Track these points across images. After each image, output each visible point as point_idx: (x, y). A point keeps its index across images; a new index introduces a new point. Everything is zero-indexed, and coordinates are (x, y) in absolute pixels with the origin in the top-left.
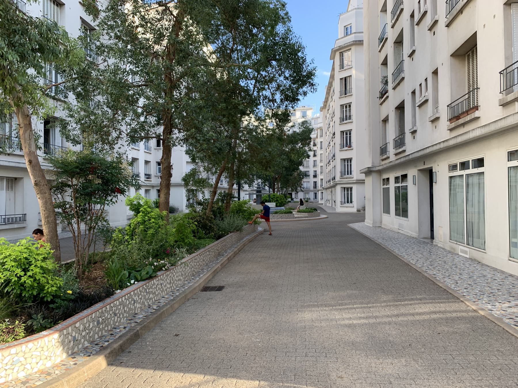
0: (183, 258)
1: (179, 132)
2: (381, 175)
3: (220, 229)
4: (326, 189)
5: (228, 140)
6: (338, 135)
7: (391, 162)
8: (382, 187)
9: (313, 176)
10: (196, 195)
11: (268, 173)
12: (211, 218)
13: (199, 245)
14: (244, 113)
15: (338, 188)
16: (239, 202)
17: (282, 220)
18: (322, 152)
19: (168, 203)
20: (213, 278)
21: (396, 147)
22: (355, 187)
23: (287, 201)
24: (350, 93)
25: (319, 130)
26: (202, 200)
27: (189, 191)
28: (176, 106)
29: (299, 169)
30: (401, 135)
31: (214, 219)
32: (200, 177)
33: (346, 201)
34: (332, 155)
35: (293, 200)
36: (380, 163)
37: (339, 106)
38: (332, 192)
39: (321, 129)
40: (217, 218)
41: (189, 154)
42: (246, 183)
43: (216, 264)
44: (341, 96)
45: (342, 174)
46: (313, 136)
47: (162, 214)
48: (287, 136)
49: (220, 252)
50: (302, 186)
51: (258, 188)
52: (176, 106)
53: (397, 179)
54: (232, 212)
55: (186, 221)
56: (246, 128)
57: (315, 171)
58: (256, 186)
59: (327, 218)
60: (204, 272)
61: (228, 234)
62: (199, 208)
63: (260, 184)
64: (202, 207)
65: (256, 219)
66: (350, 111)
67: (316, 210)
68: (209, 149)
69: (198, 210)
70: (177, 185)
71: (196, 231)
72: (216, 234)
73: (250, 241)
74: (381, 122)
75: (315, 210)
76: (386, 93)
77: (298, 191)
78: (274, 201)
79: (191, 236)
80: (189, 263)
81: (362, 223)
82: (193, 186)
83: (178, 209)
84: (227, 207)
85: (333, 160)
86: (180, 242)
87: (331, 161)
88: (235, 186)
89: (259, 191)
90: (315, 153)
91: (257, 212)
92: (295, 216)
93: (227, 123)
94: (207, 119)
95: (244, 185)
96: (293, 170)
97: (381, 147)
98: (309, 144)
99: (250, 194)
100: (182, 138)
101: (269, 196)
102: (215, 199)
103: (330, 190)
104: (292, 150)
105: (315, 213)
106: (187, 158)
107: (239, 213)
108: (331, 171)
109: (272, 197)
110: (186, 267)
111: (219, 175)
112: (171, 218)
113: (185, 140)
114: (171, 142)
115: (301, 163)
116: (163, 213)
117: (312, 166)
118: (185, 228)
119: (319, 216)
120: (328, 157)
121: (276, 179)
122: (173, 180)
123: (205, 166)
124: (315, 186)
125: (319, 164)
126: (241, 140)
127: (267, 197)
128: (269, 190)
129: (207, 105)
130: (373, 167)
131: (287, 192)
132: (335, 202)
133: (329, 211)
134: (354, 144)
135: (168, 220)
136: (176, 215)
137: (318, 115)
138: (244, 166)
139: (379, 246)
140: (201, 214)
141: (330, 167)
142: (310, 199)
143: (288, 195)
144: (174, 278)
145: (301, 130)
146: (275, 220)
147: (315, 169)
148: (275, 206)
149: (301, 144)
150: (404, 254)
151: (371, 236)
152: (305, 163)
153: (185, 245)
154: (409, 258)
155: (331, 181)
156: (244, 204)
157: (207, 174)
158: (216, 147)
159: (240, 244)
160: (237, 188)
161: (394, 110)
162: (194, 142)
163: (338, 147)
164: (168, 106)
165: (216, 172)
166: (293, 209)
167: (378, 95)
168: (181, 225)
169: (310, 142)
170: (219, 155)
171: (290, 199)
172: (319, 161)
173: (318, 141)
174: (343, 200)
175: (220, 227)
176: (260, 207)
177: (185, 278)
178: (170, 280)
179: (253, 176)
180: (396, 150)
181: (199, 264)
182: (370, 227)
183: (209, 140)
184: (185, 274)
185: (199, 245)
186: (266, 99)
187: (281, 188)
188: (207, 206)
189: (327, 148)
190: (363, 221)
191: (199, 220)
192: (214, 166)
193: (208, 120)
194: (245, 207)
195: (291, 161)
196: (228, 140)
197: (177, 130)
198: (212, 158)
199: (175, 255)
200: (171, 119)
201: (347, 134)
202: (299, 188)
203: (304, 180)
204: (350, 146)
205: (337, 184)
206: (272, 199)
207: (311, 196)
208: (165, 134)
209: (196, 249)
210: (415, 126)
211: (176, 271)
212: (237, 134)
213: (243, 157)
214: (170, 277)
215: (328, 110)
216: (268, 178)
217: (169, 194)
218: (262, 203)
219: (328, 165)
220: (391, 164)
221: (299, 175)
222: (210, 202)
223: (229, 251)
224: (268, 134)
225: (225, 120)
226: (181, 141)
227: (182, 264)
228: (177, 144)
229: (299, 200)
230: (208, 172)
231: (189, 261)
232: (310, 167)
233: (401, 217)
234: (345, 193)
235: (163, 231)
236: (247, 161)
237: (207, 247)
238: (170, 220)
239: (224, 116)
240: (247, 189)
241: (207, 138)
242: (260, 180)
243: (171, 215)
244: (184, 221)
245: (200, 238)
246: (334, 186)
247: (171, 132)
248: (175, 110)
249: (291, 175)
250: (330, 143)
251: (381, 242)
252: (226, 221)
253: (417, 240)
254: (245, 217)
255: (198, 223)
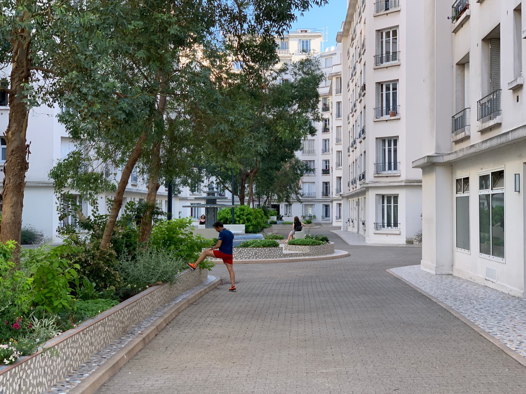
0: (48, 338)
1: (46, 77)
2: (452, 173)
3: (129, 279)
4: (348, 197)
5: (148, 97)
6: (371, 90)
7: (472, 146)
8: (455, 196)
9: (321, 172)
10: (80, 206)
11: (229, 164)
12: (111, 255)
13: (83, 312)
14: (180, 42)
15: (371, 197)
16: (169, 223)
17: (258, 260)
18: (340, 123)
19: (20, 223)
20: (110, 380)
21: (482, 117)
22: (403, 195)
23: (269, 221)
24: (395, 6)
25: (334, 79)
26: (92, 218)
27: (66, 198)
28: (38, 23)
29: (293, 156)
30: (493, 93)
31: (117, 258)
32: (90, 170)
33: (386, 221)
34: (359, 130)
35: (281, 219)
36: (451, 149)
37: (374, 33)
38: (358, 204)
39: (338, 76)
40: (122, 256)
41: (66, 122)
42: (185, 183)
43: (118, 352)
44: (377, 12)
45: (379, 169)
46: (322, 90)
47: (5, 247)
48: (270, 89)
49: (127, 326)
50: (300, 191)
51: (209, 194)
52: (38, 23)
53: (483, 179)
54: (154, 243)
55: (57, 261)
56: (184, 71)
57: (327, 162)
58: (206, 189)
59: (348, 255)
60: (91, 367)
61: (145, 289)
62: (84, 235)
63: (214, 186)
64: (91, 232)
65: (205, 258)
66: (395, 43)
67: (325, 239)
68: (105, 114)
69: (83, 238)
70: (40, 186)
71: (77, 283)
72: (120, 288)
73: (192, 303)
74: (455, 66)
75: (325, 239)
76: (465, 9)
77: (291, 200)
78: (241, 221)
79: (66, 293)
80: (61, 349)
81: (415, 266)
82: (73, 188)
83: (42, 235)
84: (143, 234)
85: (361, 139)
86: (43, 305)
87: (358, 141)
88: (163, 190)
89: (211, 201)
90: (326, 125)
91: (205, 244)
92: (285, 252)
93: (147, 61)
94: (104, 52)
95: (181, 188)
96: (283, 159)
97: (453, 117)
98: (314, 107)
99: (193, 208)
100: (50, 89)
101: (232, 210)
102: (120, 215)
103: (356, 199)
104: (280, 117)
105: (324, 246)
106: (62, 130)
107: (169, 245)
108: (358, 161)
109: (238, 213)
110: (55, 358)
111: (127, 168)
112: (23, 255)
113: (57, 94)
114: (27, 97)
115: (296, 145)
116: (8, 245)
117: (321, 151)
118: (54, 275)
119: (333, 252)
120: (351, 134)
121: (247, 175)
122: (30, 176)
123: (99, 148)
124: (326, 192)
125: (334, 147)
126: (176, 95)
127: (228, 213)
128: (233, 198)
129: (104, 23)
130: (438, 155)
131: (270, 202)
132: (363, 224)
133: (351, 242)
134: (402, 110)
135: (17, 260)
136: (35, 248)
137: (333, 48)
138: (180, 148)
139: (445, 312)
140: (88, 248)
141: (355, 155)
142: (315, 217)
143: (271, 210)
144: (27, 380)
145: (299, 77)
146: (244, 260)
147: (326, 157)
148: (244, 232)
149: (299, 108)
150: (495, 329)
151: (432, 293)
152: (305, 144)
153: (54, 312)
154: (505, 337)
155: (358, 182)
156: (180, 227)
157: (104, 165)
158: (121, 109)
159: (169, 311)
160: (166, 193)
161: (480, 42)
162: (76, 99)
163: (371, 113)
164: (23, 25)
165: (122, 160)
166: (281, 239)
167: (450, 13)
168: (46, 271)
169: (318, 101)
170: (126, 126)
171: (275, 218)
172: (334, 141)
173: (333, 100)
174: (380, 221)
175: (128, 275)
176: (213, 234)
177: (51, 381)
178: (20, 385)
179: (200, 170)
180: (483, 122)
181: (82, 352)
182: (431, 275)
183: (106, 96)
184: (52, 372)
185: (83, 312)
186: (225, 15)
187: (257, 194)
188: (103, 230)
189: (351, 115)
190: (417, 262)
191: (83, 260)
192: (118, 147)
193: (105, 54)
194: (182, 234)
195: (278, 141)
196: (148, 97)
197: (40, 72)
198: (112, 131)
199: (31, 332)
200: (28, 50)
201: (388, 89)
202: (293, 196)
203: (305, 178)
204: (395, 113)
205: (368, 188)
206: (238, 217)
207: (318, 211)
208: (16, 80)
209: (75, 321)
210: (520, 75)
211: (32, 366)
212: (166, 83)
213: (178, 130)
214: (21, 378)
215: (353, 40)
216: (230, 173)
217: (22, 206)
218: (218, 225)
219: (351, 149)
220: (473, 150)
221: (293, 168)
222: (108, 221)
223: (145, 324)
224: (230, 85)
225: (141, 54)
226: (48, 96)
227: (45, 350)
228: (40, 101)
229: (292, 220)
230: (105, 160)
231: (62, 345)
232: (316, 152)
233: (491, 256)
234: (383, 207)
235: (7, 283)
236: (186, 140)
237: (99, 317)
238: (22, 259)
239: (140, 46)
240: (188, 196)
241: (101, 91)
242: (213, 179)
243: (24, 248)
244: (52, 263)
245: (85, 297)
246: (363, 192)
247: (27, 77)
248: (37, 31)
249: (278, 169)
250: (355, 105)
251: (450, 305)
252: (142, 261)
253: (521, 303)
254: (182, 253)
255: (81, 265)
